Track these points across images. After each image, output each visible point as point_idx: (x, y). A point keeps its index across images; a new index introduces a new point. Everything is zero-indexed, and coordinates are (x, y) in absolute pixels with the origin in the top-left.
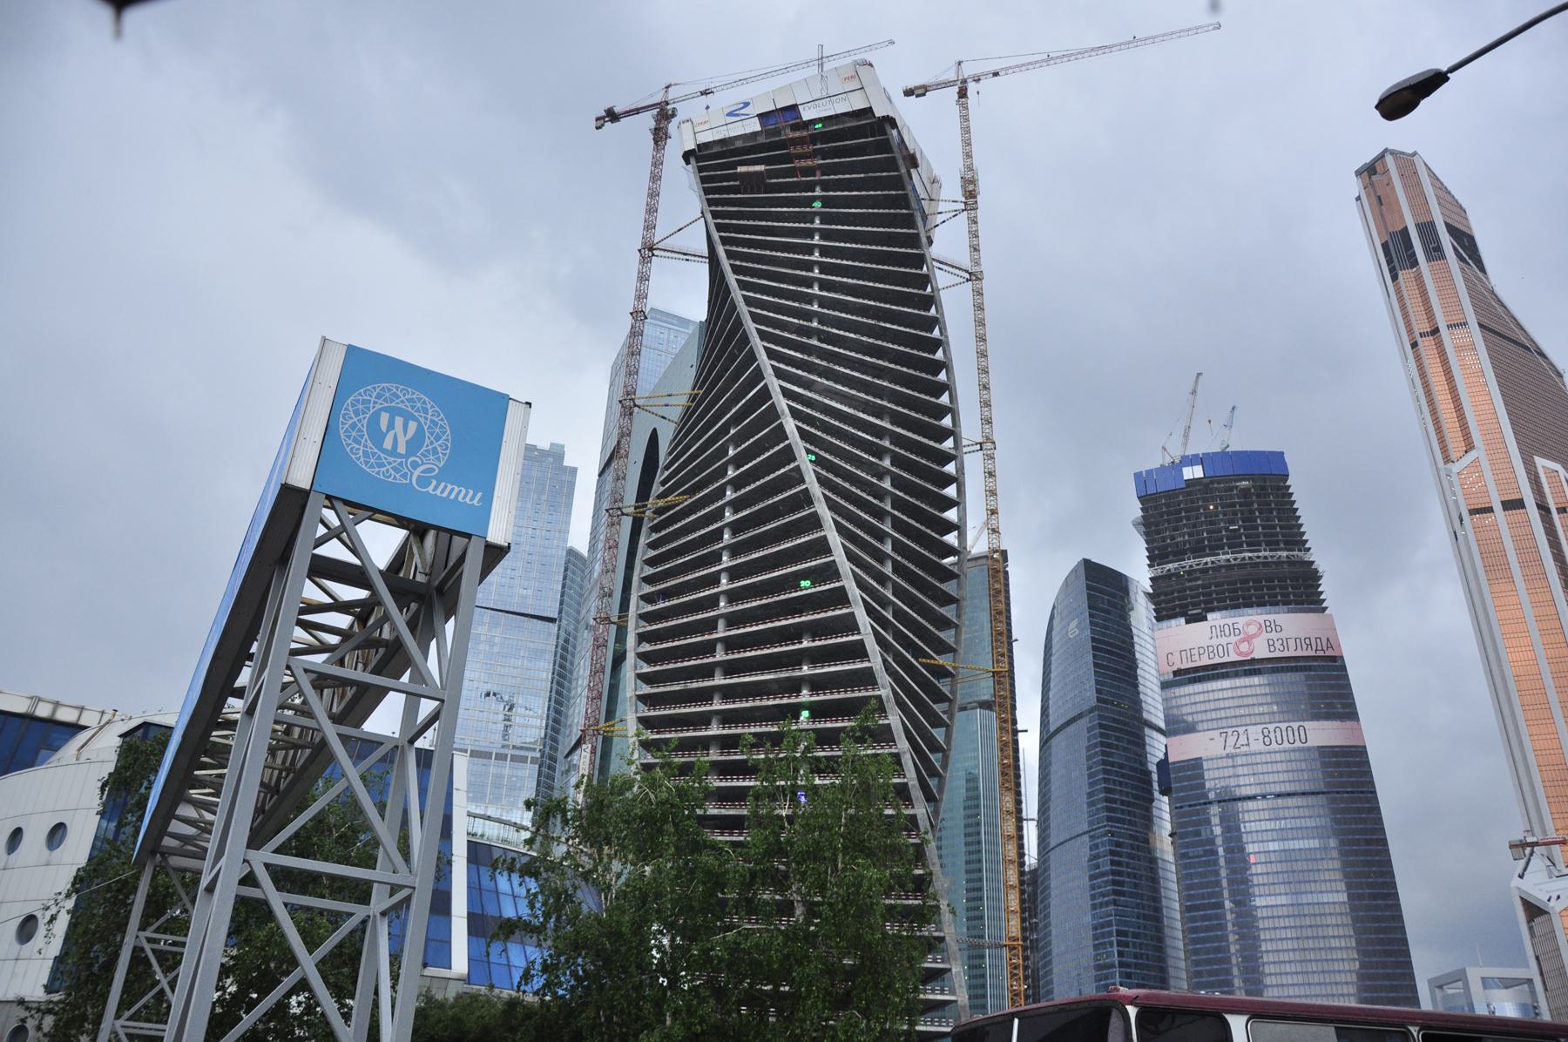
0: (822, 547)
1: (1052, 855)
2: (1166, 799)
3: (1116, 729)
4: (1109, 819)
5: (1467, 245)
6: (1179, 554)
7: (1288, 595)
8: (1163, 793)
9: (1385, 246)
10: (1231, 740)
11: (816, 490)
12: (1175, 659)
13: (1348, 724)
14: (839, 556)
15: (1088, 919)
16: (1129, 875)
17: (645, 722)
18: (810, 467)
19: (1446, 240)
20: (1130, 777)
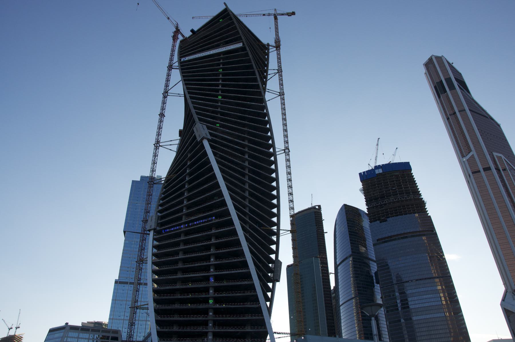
8: (378, 283)
9: (435, 87)
19: (456, 84)
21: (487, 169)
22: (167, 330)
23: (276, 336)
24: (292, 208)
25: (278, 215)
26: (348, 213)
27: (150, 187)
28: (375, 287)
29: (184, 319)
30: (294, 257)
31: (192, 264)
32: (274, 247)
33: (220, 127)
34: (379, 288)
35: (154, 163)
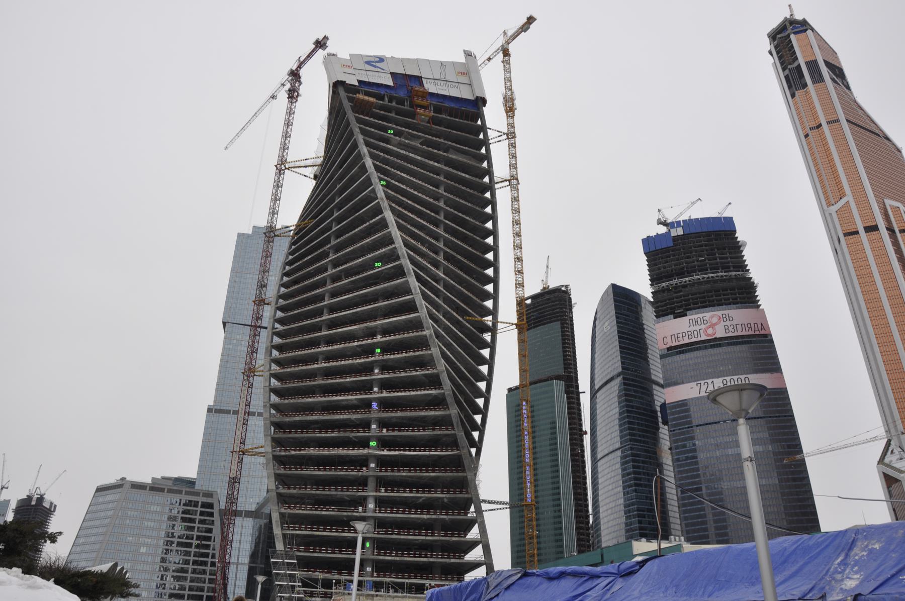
0: (389, 240)
1: (599, 464)
2: (666, 427)
3: (634, 386)
4: (631, 440)
5: (838, 73)
6: (669, 277)
7: (736, 299)
8: (665, 422)
9: (787, 77)
10: (704, 388)
11: (385, 204)
12: (668, 340)
13: (775, 375)
14: (399, 243)
15: (622, 501)
16: (644, 474)
17: (706, 530)
18: (381, 187)
20: (643, 414)
21: (872, 229)
22: (295, 491)
23: (484, 506)
24: (520, 285)
25: (495, 297)
26: (622, 300)
27: (269, 242)
28: (661, 430)
29: (325, 473)
30: (522, 371)
31: (341, 378)
32: (486, 353)
33: (394, 134)
34: (667, 432)
35: (276, 199)
